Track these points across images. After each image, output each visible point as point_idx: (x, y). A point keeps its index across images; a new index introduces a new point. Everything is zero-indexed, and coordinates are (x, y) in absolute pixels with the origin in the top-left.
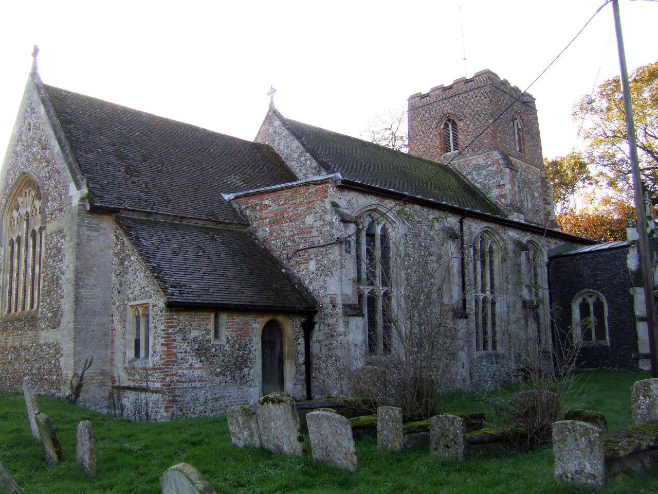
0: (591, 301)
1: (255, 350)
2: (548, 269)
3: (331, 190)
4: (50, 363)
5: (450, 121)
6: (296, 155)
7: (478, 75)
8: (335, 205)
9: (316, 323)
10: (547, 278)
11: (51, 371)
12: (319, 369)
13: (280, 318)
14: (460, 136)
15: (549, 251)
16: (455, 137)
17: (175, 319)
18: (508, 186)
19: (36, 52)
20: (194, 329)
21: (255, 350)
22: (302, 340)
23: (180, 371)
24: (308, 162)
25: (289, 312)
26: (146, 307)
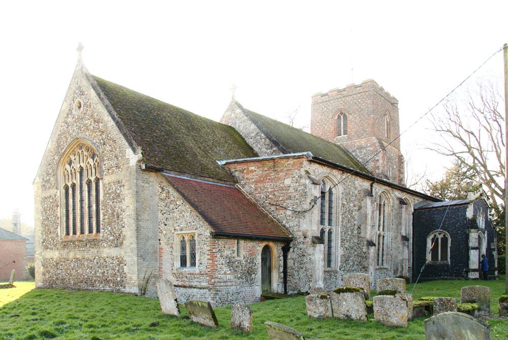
0: (440, 237)
1: (258, 264)
2: (413, 216)
3: (305, 163)
4: (114, 269)
8: (307, 172)
9: (291, 247)
10: (412, 222)
11: (115, 274)
12: (293, 276)
13: (271, 244)
15: (415, 205)
16: (345, 125)
17: (216, 243)
18: (381, 161)
19: (80, 48)
20: (226, 250)
21: (258, 264)
22: (282, 258)
23: (219, 276)
24: (263, 140)
25: (275, 240)
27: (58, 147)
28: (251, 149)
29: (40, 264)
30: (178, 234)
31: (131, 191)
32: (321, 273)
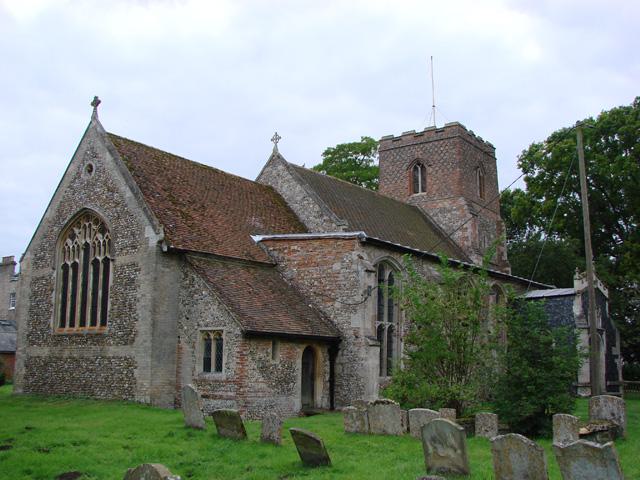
5: (418, 165)
6: (299, 198)
7: (448, 127)
12: (341, 385)
13: (314, 345)
14: (429, 180)
16: (424, 179)
19: (96, 102)
22: (328, 363)
26: (219, 333)
27: (59, 217)
28: (296, 218)
29: (22, 364)
30: (202, 331)
31: (148, 277)
32: (376, 384)
